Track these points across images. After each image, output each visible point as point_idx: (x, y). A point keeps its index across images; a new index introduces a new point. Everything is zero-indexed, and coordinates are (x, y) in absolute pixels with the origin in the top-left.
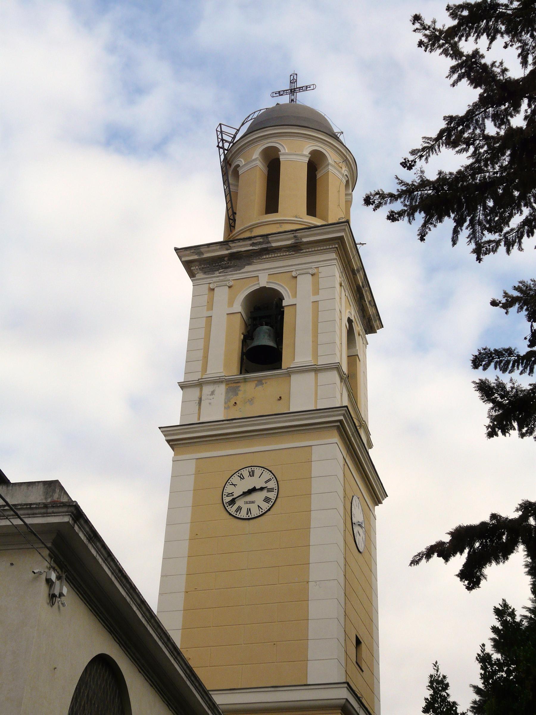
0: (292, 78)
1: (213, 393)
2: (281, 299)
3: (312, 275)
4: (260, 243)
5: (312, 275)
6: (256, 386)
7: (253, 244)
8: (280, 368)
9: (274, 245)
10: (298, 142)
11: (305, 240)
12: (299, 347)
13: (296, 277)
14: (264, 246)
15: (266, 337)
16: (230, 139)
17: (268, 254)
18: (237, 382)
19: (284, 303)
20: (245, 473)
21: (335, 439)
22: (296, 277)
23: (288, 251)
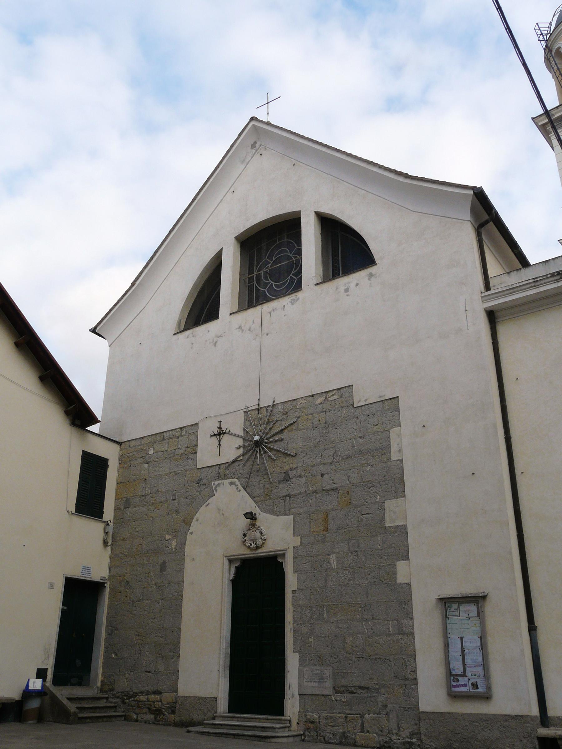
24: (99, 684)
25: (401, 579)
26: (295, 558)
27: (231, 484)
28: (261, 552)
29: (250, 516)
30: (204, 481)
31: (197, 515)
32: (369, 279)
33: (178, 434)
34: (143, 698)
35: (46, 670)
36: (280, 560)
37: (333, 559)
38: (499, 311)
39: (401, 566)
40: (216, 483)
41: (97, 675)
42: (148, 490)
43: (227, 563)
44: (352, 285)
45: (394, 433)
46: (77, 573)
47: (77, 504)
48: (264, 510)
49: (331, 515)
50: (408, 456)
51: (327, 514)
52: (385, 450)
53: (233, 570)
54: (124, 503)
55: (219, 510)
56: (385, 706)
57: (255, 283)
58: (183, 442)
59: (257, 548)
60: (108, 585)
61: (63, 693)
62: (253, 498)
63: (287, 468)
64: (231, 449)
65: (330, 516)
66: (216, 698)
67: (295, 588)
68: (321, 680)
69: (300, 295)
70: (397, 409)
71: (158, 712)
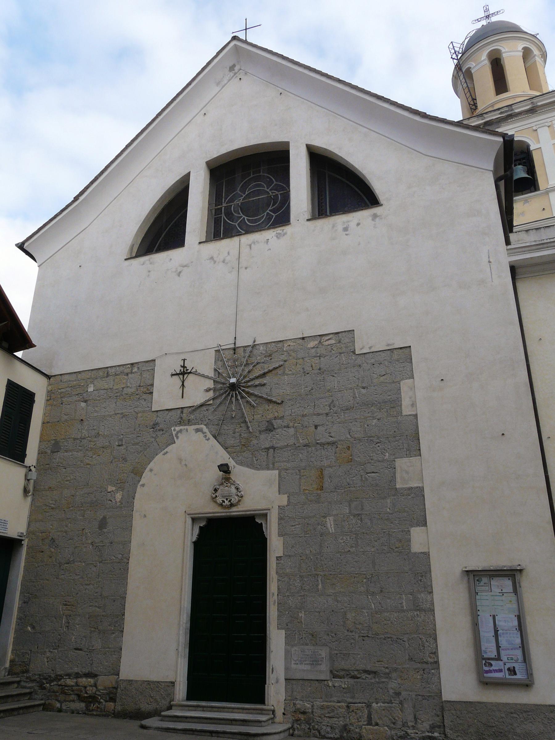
0: (485, 8)
2: (528, 146)
3: (549, 127)
4: (506, 112)
5: (549, 127)
6: (524, 204)
7: (500, 114)
8: (539, 190)
9: (516, 111)
10: (511, 43)
11: (539, 104)
13: (536, 130)
15: (522, 172)
17: (512, 118)
19: (531, 148)
22: (536, 130)
23: (526, 114)
24: (7, 665)
26: (280, 519)
27: (197, 430)
28: (235, 511)
34: (70, 682)
36: (258, 521)
37: (330, 522)
38: (521, 267)
40: (178, 428)
43: (189, 521)
48: (241, 464)
50: (423, 410)
52: (395, 403)
53: (197, 531)
54: (52, 447)
55: (180, 460)
56: (398, 694)
57: (223, 215)
58: (133, 381)
59: (232, 505)
60: (25, 543)
62: (226, 448)
63: (271, 416)
64: (198, 392)
65: (326, 473)
66: (173, 683)
67: (281, 554)
68: (315, 662)
69: (287, 229)
70: (410, 360)
71: (92, 699)
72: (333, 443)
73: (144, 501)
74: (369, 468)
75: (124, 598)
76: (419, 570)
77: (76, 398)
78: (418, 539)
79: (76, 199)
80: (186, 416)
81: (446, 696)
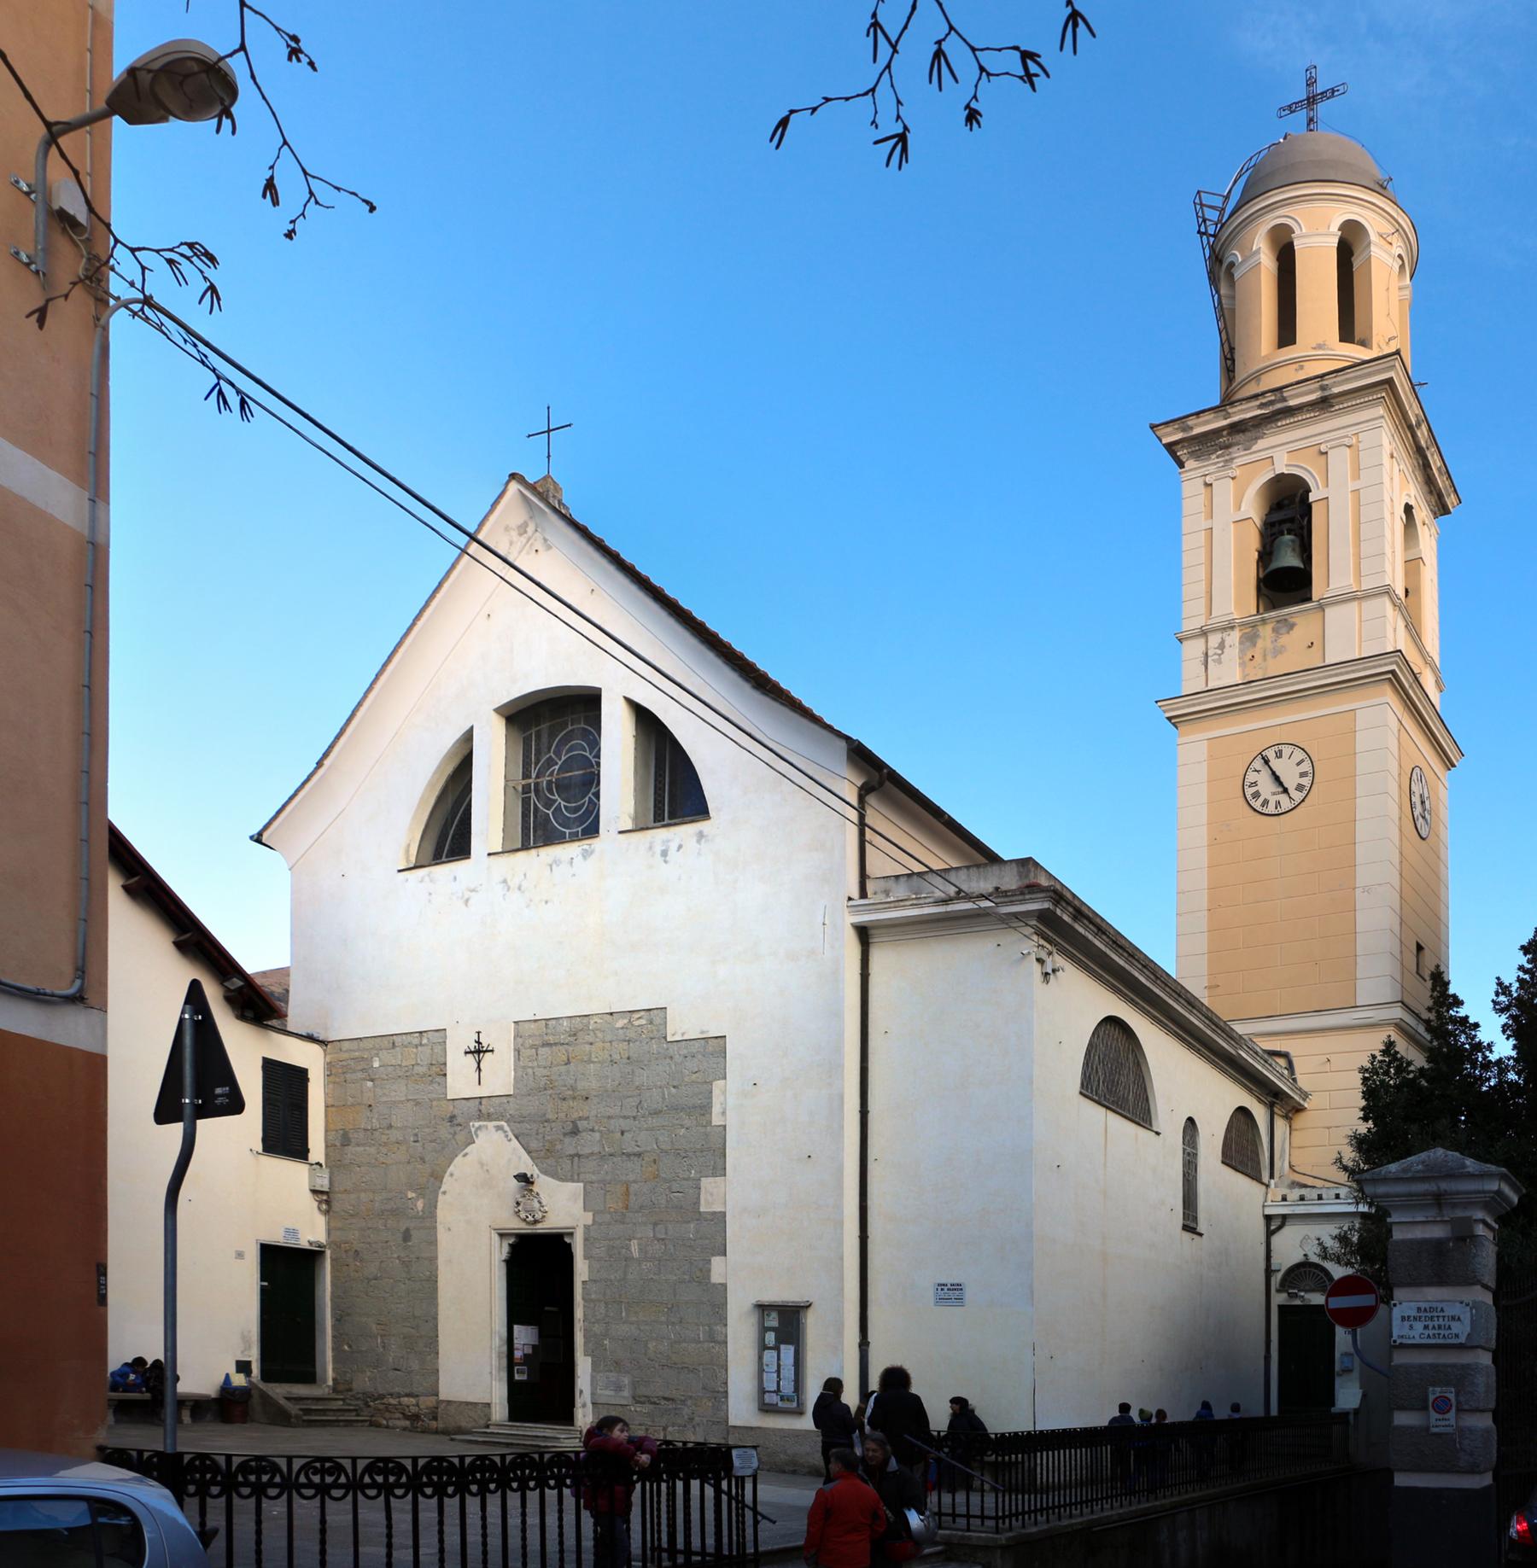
1: (1222, 646)
4: (1271, 403)
7: (1262, 406)
8: (1309, 599)
9: (1292, 403)
11: (1336, 390)
12: (1334, 569)
14: (1279, 406)
16: (1218, 202)
18: (1253, 625)
19: (1312, 497)
20: (1306, 781)
21: (1389, 695)
24: (330, 1383)
25: (716, 1277)
26: (586, 1240)
27: (499, 1128)
28: (541, 1228)
29: (524, 1179)
30: (459, 1120)
31: (451, 1168)
32: (699, 842)
33: (416, 1041)
34: (393, 1401)
35: (249, 1363)
36: (567, 1240)
37: (634, 1246)
38: (874, 928)
39: (716, 1261)
40: (477, 1124)
41: (325, 1371)
42: (376, 1124)
43: (496, 1238)
44: (673, 846)
45: (718, 1085)
46: (277, 1238)
47: (264, 1140)
48: (545, 1172)
49: (634, 1187)
50: (732, 1123)
51: (627, 1185)
52: (705, 1108)
53: (506, 1249)
54: (339, 1141)
55: (482, 1165)
56: (692, 1419)
57: (533, 795)
58: (424, 1055)
59: (536, 1222)
60: (328, 1253)
61: (278, 1391)
62: (529, 1153)
63: (575, 1116)
64: (499, 1077)
65: (632, 1189)
66: (489, 1405)
67: (586, 1278)
68: (619, 1388)
69: (595, 843)
70: (723, 1053)
71: (415, 1417)
72: (639, 1155)
73: (445, 1213)
74: (675, 1187)
75: (435, 1318)
76: (716, 1301)
77: (360, 1075)
78: (718, 1269)
79: (320, 764)
80: (483, 1109)
81: (732, 1422)
